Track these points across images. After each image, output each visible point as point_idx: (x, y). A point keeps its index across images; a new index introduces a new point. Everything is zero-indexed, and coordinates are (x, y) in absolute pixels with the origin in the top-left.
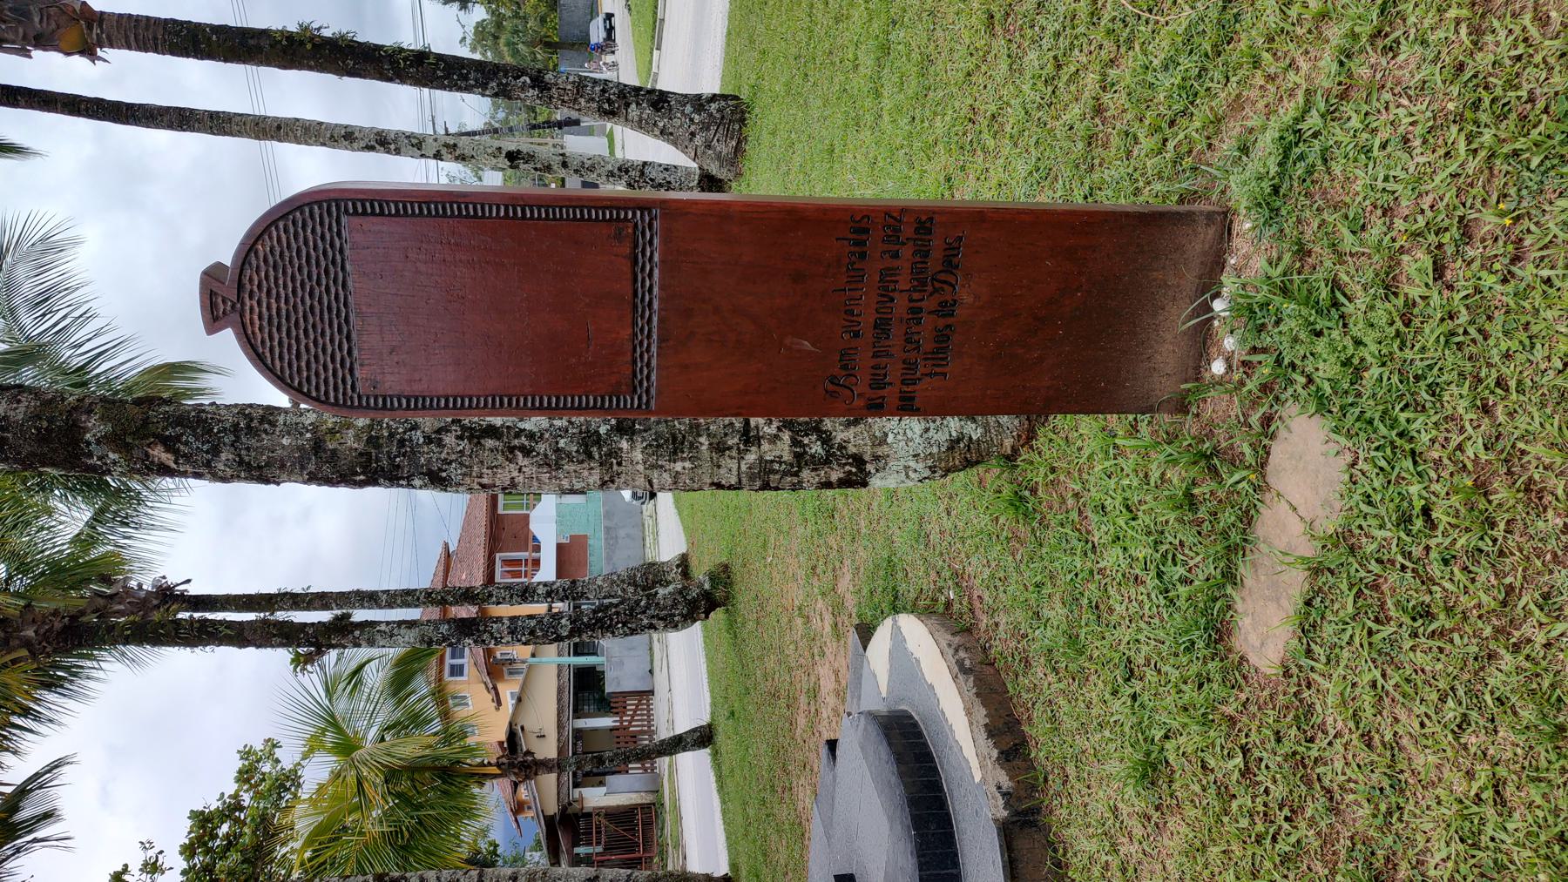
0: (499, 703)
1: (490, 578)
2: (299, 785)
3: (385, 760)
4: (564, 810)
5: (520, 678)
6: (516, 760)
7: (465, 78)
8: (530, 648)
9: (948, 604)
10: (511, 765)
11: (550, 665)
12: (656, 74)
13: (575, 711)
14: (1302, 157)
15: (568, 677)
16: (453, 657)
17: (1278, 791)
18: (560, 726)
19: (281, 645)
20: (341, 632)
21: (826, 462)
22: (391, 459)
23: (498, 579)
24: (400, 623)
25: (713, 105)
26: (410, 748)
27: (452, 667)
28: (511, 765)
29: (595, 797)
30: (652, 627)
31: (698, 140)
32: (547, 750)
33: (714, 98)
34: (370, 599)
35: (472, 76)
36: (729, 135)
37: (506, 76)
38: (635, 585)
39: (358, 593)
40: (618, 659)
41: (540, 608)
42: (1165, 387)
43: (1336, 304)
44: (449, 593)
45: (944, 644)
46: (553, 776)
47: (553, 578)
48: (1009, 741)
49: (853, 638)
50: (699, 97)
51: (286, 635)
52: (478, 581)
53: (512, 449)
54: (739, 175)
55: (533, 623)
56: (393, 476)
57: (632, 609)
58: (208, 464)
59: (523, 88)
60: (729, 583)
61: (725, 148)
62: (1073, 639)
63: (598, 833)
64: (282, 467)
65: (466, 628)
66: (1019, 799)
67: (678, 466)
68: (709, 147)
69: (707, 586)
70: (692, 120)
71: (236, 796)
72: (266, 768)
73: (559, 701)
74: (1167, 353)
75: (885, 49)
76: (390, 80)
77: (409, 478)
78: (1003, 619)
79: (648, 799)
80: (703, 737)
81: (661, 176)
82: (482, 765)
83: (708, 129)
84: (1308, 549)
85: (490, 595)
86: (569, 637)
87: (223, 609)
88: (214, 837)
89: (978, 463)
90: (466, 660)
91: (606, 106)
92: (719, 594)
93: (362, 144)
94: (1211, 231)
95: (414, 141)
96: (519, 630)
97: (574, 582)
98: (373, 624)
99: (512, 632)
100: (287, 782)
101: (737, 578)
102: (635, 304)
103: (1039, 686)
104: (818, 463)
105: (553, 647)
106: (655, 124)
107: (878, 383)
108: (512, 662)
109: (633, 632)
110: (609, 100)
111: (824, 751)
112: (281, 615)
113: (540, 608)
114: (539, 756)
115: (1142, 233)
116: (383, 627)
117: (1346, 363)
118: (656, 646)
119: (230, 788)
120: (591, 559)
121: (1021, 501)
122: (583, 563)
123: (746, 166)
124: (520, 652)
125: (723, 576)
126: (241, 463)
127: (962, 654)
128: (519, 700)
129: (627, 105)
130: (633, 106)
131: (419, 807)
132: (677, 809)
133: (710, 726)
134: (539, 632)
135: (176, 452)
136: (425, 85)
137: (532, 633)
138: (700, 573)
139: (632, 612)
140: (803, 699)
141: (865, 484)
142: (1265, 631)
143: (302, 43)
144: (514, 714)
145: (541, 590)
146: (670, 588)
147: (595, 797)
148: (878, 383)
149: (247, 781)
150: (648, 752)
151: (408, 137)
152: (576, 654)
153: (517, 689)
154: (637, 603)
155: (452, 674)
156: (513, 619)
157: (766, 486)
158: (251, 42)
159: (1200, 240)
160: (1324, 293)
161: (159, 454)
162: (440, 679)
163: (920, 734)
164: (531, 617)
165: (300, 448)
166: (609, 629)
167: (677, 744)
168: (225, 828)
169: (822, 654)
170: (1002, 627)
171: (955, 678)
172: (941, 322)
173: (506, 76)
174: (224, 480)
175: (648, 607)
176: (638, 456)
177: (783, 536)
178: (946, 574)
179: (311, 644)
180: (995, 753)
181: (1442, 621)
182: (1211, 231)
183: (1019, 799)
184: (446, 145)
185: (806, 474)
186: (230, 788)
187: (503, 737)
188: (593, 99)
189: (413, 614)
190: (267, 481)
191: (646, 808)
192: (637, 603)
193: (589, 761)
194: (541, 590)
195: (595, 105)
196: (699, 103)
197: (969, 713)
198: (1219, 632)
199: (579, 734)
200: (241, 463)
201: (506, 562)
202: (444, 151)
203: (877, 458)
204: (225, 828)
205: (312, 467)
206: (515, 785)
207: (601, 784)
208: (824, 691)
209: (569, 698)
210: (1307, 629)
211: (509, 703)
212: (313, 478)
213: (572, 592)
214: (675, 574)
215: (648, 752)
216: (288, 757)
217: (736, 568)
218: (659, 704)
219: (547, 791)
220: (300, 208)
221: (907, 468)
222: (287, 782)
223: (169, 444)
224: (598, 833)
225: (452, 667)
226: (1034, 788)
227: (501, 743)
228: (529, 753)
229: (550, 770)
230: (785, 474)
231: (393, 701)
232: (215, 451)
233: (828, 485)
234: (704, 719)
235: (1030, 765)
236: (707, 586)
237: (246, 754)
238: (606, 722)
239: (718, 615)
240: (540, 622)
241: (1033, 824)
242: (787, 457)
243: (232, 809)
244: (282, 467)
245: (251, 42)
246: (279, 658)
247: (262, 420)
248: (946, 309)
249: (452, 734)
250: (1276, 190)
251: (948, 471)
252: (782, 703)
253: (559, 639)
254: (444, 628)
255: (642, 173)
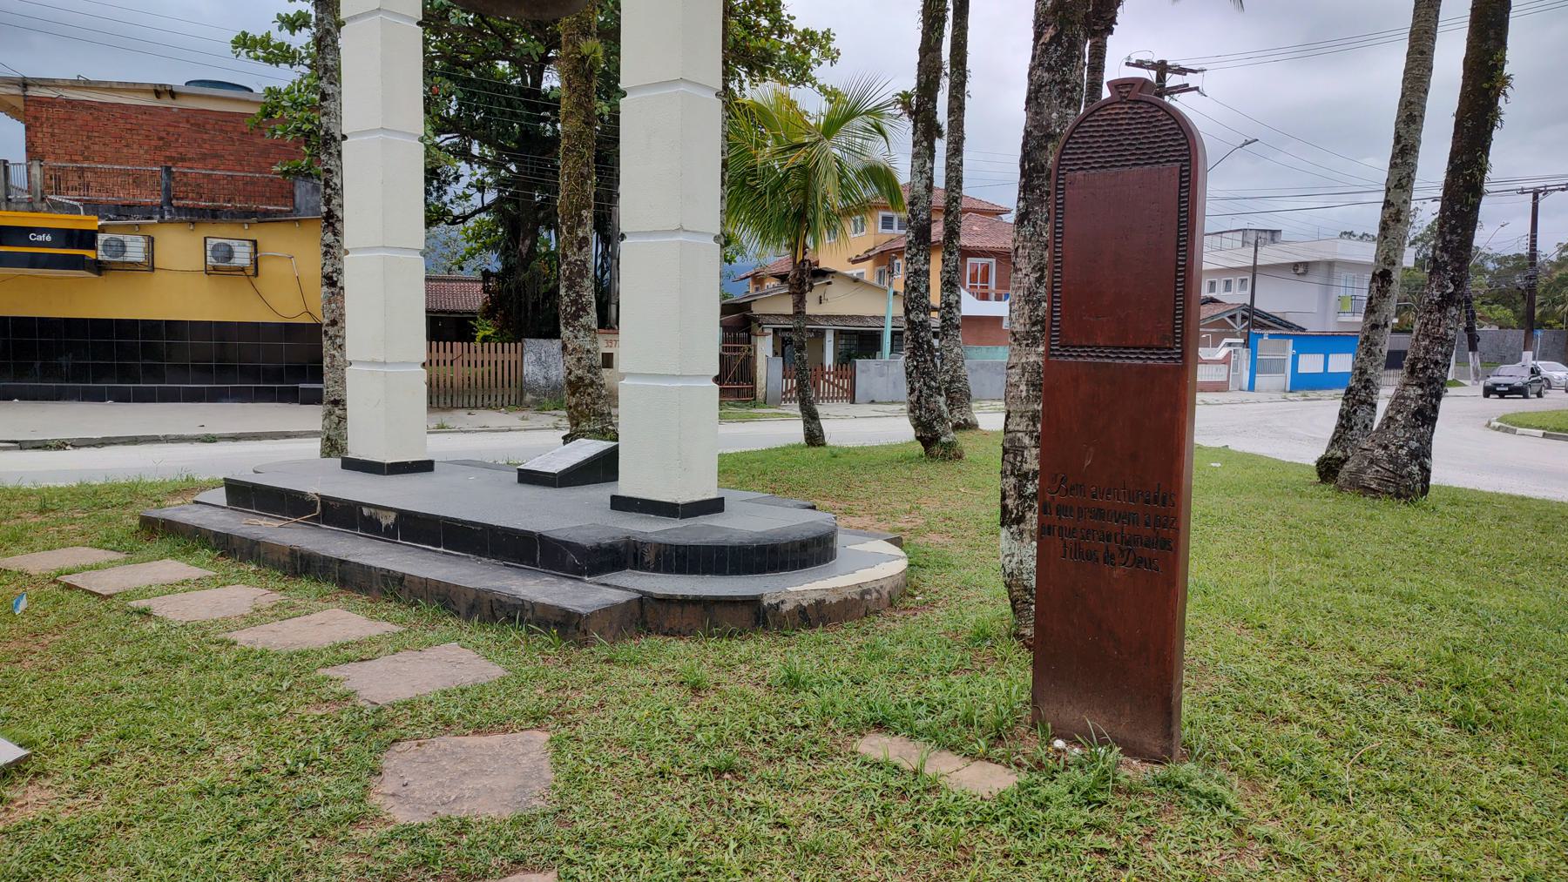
0: (854, 262)
1: (967, 253)
2: (797, 84)
3: (822, 168)
4: (755, 319)
5: (875, 282)
6: (805, 277)
7: (1453, 231)
8: (901, 289)
9: (913, 596)
10: (802, 272)
11: (886, 310)
12: (1514, 432)
13: (841, 332)
14: (1199, 803)
15: (871, 326)
16: (900, 220)
17: (781, 739)
18: (828, 317)
19: (919, 83)
20: (926, 129)
21: (1020, 496)
22: (1038, 187)
23: (970, 260)
24: (931, 179)
25: (1416, 469)
26: (828, 186)
27: (891, 219)
28: (802, 272)
29: (764, 347)
30: (912, 390)
31: (1379, 452)
32: (811, 308)
33: (1426, 471)
34: (956, 150)
35: (1454, 237)
36: (1383, 481)
37: (1454, 270)
38: (951, 382)
39: (962, 138)
40: (885, 373)
41: (935, 298)
42: (1049, 711)
43: (1089, 803)
44: (956, 217)
45: (884, 583)
46: (790, 311)
47: (964, 313)
48: (812, 615)
49: (892, 536)
50: (1429, 456)
51: (927, 87)
52: (964, 241)
53: (1042, 270)
54: (1341, 489)
55: (922, 290)
56: (1027, 187)
57: (928, 374)
58: (1041, 64)
59: (1441, 286)
60: (944, 458)
61: (1369, 477)
62: (881, 656)
63: (735, 349)
64: (1037, 114)
65: (922, 234)
66: (774, 615)
67: (1023, 387)
68: (1372, 462)
69: (943, 439)
70: (1401, 447)
71: (791, 30)
72: (814, 54)
73: (852, 317)
74: (1071, 714)
75: (1409, 599)
76: (1451, 161)
77: (1024, 199)
78: (897, 625)
79: (760, 394)
80: (814, 438)
81: (1359, 422)
82: (805, 247)
83: (1390, 462)
84: (929, 771)
85: (951, 254)
86: (909, 321)
87: (955, 24)
88: (758, 14)
89: (1014, 610)
90: (896, 231)
91: (1420, 365)
92: (936, 449)
93: (1402, 132)
94: (1157, 750)
95: (1404, 182)
96: (918, 276)
97: (957, 327)
98: (932, 157)
99: (916, 272)
100: (802, 76)
101: (949, 465)
102: (1119, 347)
103: (849, 638)
104: (1019, 489)
105: (901, 311)
106: (1399, 412)
107: (1061, 510)
108: (891, 273)
109: (909, 375)
110: (1426, 368)
111: (809, 503)
112: (945, 83)
113: (935, 298)
114: (808, 296)
115: (1163, 706)
116: (928, 165)
117: (1047, 799)
118: (897, 407)
119: (799, 26)
120: (984, 348)
121: (982, 635)
122: (981, 341)
123: (1348, 496)
124: (899, 282)
125: (952, 454)
126: (1041, 86)
127: (875, 595)
128: (856, 280)
129: (1421, 386)
130: (1420, 392)
131: (774, 193)
132: (751, 418)
133: (824, 445)
134: (914, 298)
135: (1050, 44)
136: (1445, 194)
137: (915, 289)
138: (962, 438)
139: (925, 374)
140: (844, 506)
141: (1002, 525)
142: (875, 746)
143: (1490, 79)
144: (844, 276)
145: (953, 298)
146: (944, 408)
147: (764, 347)
148: (1061, 510)
149: (804, 39)
150: (805, 393)
151: (1409, 176)
152: (893, 334)
153: (866, 278)
154: (934, 379)
155: (884, 218)
156: (927, 273)
157: (1005, 451)
158: (1491, 33)
159: (1154, 745)
160: (1100, 797)
161: (1049, 33)
162: (877, 207)
163: (819, 563)
164: (928, 288)
165: (1049, 125)
166: (913, 355)
167: (810, 417)
168: (765, 23)
169: (879, 521)
170: (889, 631)
171: (859, 585)
172: (1100, 555)
173: (1454, 270)
174: (1030, 74)
175: (929, 388)
176: (1032, 359)
177: (975, 488)
178: (935, 597)
179: (920, 108)
180: (805, 604)
181: (879, 819)
182: (1157, 750)
183: (774, 615)
184: (1399, 212)
185: (1012, 480)
186: (799, 26)
187: (821, 266)
188: (1428, 353)
189: (940, 181)
190: (1028, 102)
191: (752, 393)
192: (934, 379)
193: (796, 343)
194: (953, 298)
195: (1421, 354)
196: (1422, 454)
197: (834, 590)
198: (881, 726)
199: (820, 334)
200: (1041, 86)
201: (986, 268)
202: (1392, 210)
203: (1021, 533)
204: (765, 23)
205: (1036, 133)
206: (782, 278)
207: (775, 354)
208: (849, 519)
209: (853, 326)
210: (878, 765)
211: (854, 271)
212: (1028, 134)
213: (952, 323)
214: (958, 417)
215: (805, 393)
216: (823, 73)
217: (958, 465)
218: (843, 407)
219: (776, 304)
220: (1185, 137)
221: (1013, 555)
222: (802, 76)
223: (1056, 39)
224: (735, 349)
225: (891, 219)
226: (780, 627)
227: (817, 264)
228: (812, 287)
229: (795, 306)
230: (1013, 465)
231: (860, 169)
232: (1049, 69)
233: (1004, 498)
234: (829, 441)
235: (796, 628)
236: (943, 439)
237: (827, 36)
238: (829, 359)
239: (919, 447)
240: (923, 296)
241: (757, 623)
242: (1026, 467)
243: (780, 27)
244: (1037, 114)
245: (1491, 33)
246: (909, 83)
247: (1071, 99)
248: (1109, 558)
249: (834, 220)
250: (1180, 786)
251: (1008, 586)
252: (842, 491)
253: (907, 312)
254: (924, 215)
255: (1362, 403)
